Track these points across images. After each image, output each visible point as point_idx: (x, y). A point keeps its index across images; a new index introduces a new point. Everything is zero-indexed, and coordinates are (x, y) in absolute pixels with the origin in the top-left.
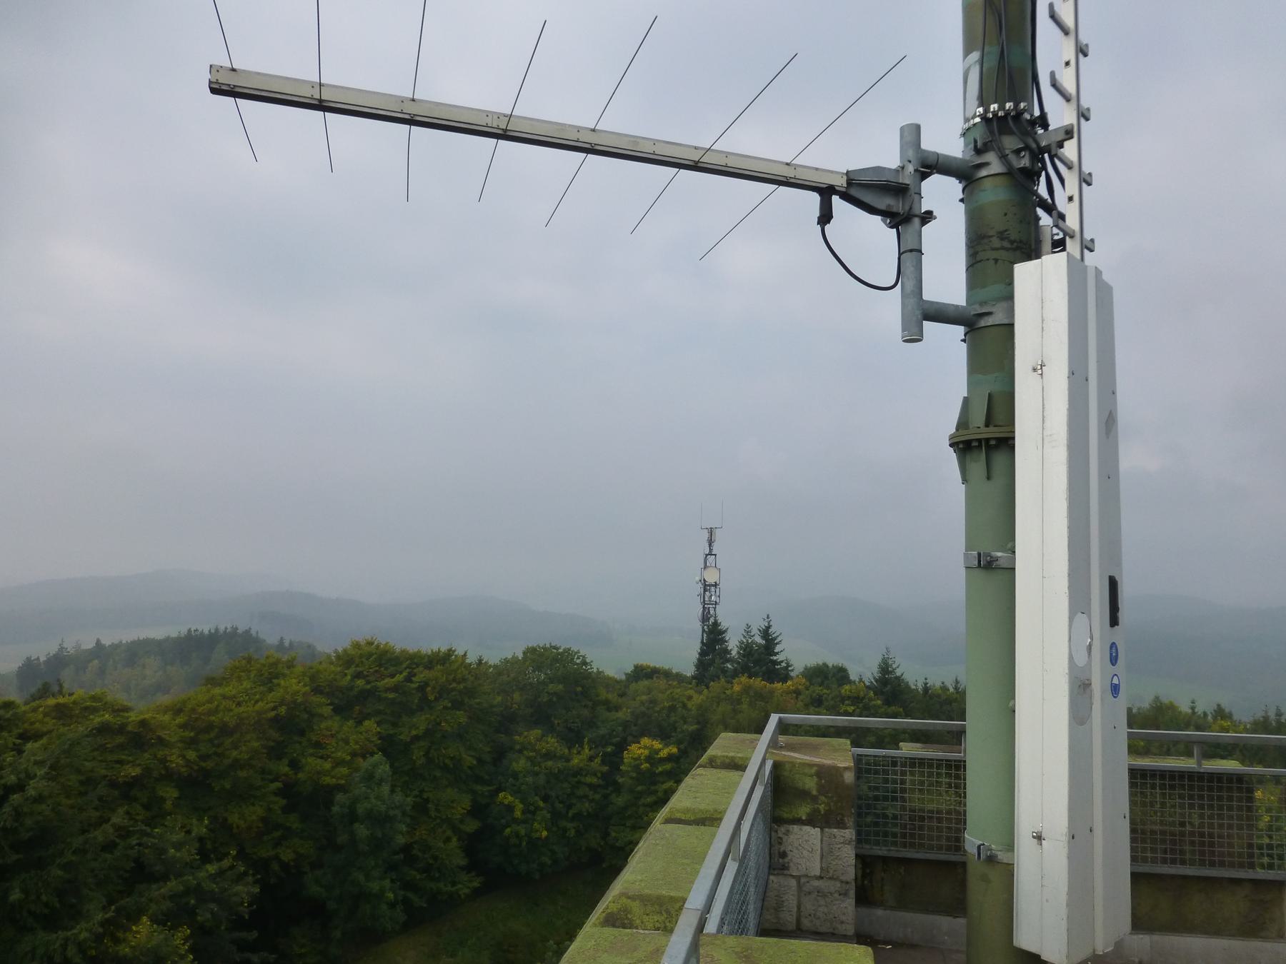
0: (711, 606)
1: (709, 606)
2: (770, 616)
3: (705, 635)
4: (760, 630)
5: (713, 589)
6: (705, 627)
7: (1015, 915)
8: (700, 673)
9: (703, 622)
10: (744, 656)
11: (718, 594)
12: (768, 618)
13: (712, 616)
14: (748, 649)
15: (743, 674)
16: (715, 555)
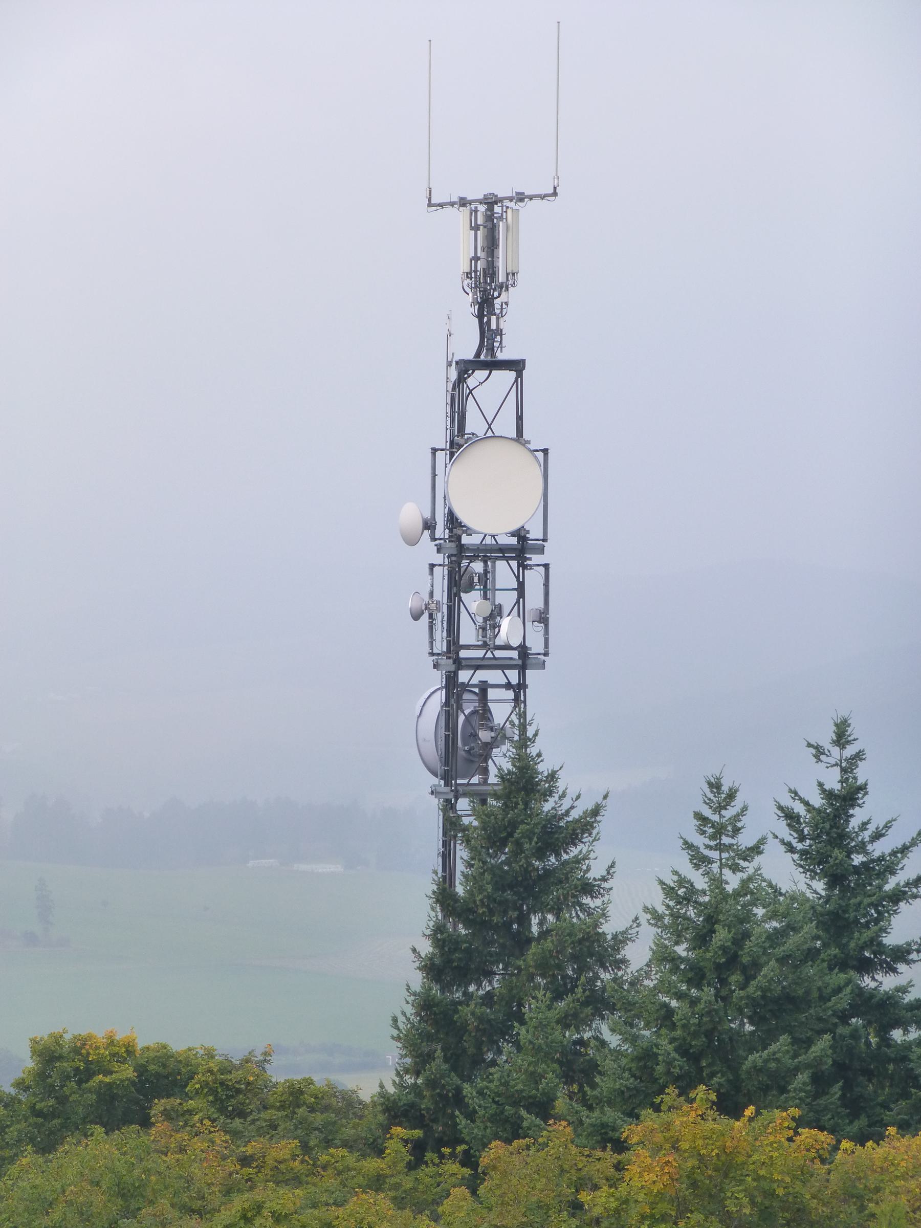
0: (494, 676)
1: (482, 675)
2: (855, 730)
3: (462, 853)
4: (791, 817)
5: (504, 573)
6: (463, 804)
7: (446, 577)
8: (432, 1083)
9: (447, 778)
10: (696, 976)
11: (534, 600)
12: (841, 737)
13: (500, 736)
14: (722, 936)
15: (685, 1085)
16: (517, 366)
